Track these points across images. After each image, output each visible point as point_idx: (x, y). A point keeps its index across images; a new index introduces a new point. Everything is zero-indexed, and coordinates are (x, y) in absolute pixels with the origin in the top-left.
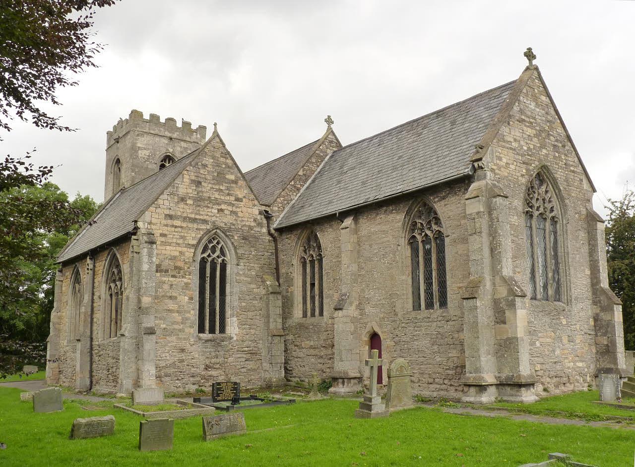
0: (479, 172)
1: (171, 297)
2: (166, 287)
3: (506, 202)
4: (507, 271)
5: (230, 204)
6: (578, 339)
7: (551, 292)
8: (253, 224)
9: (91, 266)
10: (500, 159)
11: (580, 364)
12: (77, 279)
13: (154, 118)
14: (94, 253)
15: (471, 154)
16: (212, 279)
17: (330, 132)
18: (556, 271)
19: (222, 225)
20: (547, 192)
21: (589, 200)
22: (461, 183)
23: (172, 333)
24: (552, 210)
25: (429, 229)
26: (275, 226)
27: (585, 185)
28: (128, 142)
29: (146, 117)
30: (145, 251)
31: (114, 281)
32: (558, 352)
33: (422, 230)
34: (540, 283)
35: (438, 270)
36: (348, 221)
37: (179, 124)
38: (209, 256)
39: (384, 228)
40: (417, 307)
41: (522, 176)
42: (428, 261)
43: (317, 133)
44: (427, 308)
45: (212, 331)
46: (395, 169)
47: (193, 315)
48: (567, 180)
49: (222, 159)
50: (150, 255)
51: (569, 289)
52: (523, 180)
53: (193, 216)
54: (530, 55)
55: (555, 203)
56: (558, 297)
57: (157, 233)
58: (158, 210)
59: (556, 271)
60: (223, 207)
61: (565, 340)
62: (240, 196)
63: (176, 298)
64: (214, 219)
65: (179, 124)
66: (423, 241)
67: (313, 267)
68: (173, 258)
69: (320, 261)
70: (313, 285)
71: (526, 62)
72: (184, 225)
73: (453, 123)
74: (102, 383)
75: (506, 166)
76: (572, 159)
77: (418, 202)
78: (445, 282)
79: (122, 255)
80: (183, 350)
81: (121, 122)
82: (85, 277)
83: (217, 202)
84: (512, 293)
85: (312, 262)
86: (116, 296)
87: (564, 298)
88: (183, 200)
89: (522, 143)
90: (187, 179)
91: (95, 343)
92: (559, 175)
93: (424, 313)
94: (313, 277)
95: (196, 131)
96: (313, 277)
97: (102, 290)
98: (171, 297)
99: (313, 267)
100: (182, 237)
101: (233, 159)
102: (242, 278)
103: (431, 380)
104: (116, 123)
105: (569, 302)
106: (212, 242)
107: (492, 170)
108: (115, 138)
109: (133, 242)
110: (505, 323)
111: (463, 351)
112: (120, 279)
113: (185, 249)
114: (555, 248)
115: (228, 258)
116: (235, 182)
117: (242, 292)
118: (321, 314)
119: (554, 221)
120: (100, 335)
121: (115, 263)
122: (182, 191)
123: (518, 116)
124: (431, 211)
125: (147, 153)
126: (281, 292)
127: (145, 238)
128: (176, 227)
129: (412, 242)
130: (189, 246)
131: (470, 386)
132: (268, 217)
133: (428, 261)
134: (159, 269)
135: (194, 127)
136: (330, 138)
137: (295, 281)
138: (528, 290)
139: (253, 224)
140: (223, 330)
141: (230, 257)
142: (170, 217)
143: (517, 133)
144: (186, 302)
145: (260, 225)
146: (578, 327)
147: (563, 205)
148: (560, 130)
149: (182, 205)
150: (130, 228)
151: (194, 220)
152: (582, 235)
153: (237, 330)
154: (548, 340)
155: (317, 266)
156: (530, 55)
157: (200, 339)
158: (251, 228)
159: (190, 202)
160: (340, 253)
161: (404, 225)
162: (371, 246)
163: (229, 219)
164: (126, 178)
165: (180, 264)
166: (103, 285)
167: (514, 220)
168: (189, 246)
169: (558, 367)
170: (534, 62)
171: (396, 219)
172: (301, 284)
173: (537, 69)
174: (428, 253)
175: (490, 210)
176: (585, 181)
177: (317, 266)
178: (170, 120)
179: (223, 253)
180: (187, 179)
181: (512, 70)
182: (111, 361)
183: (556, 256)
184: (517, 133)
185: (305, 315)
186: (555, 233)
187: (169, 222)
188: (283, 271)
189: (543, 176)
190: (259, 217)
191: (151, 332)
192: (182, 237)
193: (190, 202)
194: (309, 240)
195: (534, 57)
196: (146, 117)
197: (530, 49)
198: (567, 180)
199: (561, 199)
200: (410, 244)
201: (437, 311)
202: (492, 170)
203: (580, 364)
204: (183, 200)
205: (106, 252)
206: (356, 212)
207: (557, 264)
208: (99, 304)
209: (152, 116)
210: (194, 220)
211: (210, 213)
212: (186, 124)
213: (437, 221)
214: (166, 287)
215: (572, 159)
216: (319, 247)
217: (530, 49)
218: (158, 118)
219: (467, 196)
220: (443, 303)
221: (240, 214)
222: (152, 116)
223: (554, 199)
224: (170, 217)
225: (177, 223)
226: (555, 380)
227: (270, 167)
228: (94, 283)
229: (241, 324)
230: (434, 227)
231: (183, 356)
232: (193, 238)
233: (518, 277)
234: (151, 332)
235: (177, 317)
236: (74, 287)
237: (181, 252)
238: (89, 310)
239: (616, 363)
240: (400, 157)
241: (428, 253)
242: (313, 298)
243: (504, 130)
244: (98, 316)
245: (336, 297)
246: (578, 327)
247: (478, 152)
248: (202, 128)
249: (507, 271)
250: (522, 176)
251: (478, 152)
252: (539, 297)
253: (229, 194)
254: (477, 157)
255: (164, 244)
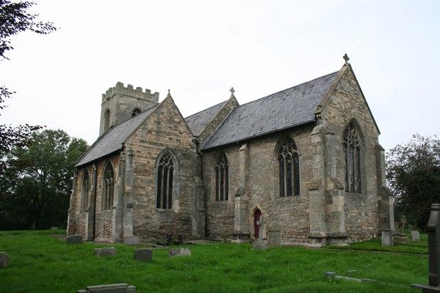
0: (320, 120)
1: (142, 187)
2: (139, 181)
3: (333, 137)
4: (334, 175)
5: (176, 135)
6: (370, 214)
7: (356, 188)
8: (189, 147)
9: (95, 169)
10: (330, 113)
11: (371, 228)
12: (86, 177)
13: (130, 87)
14: (97, 162)
15: (315, 110)
16: (164, 177)
17: (233, 97)
18: (359, 177)
19: (171, 147)
20: (354, 133)
21: (377, 138)
22: (307, 127)
23: (143, 207)
24: (357, 143)
25: (290, 151)
26: (201, 148)
27: (375, 130)
28: (115, 100)
29: (126, 86)
30: (128, 161)
31: (109, 178)
32: (359, 221)
33: (286, 152)
34: (350, 183)
35: (284, 190)
36: (244, 147)
37: (144, 91)
38: (164, 164)
39: (264, 150)
40: (282, 195)
41: (342, 123)
42: (289, 169)
43: (226, 97)
44: (288, 196)
45: (164, 207)
46: (271, 118)
47: (154, 197)
48: (365, 127)
49: (172, 110)
50: (131, 163)
51: (366, 186)
52: (342, 126)
53: (155, 141)
54: (346, 58)
55: (359, 139)
56: (359, 191)
57: (135, 150)
58: (136, 138)
59: (359, 177)
60: (172, 137)
61: (363, 214)
62: (182, 131)
63: (144, 188)
64: (167, 143)
65: (144, 91)
66: (286, 158)
67: (222, 173)
68: (144, 165)
69: (227, 169)
70: (222, 183)
71: (344, 62)
72: (150, 146)
73: (304, 93)
74: (101, 235)
75: (334, 118)
76: (368, 115)
77: (284, 138)
78: (299, 181)
79: (114, 163)
80: (148, 218)
81: (111, 89)
82: (91, 176)
83: (169, 134)
84: (336, 186)
85: (222, 170)
86: (110, 187)
87: (363, 191)
88: (150, 132)
89: (343, 105)
90: (152, 121)
91: (97, 213)
92: (361, 123)
93: (287, 199)
94: (222, 178)
95: (153, 95)
96: (222, 178)
97: (101, 183)
98: (142, 187)
99: (222, 173)
100: (149, 153)
101: (178, 110)
102: (182, 177)
103: (290, 236)
104: (108, 90)
105: (366, 194)
106: (166, 157)
107: (326, 119)
108: (107, 98)
109: (122, 155)
110: (332, 203)
111: (308, 219)
112: (113, 177)
113: (150, 160)
114: (359, 164)
115: (174, 166)
116: (179, 123)
117: (181, 186)
118: (227, 199)
119: (358, 149)
120: (100, 208)
121: (110, 168)
122: (150, 127)
123: (340, 90)
124: (291, 141)
125: (126, 106)
126: (203, 189)
127: (129, 153)
128: (145, 147)
129: (280, 158)
130: (152, 158)
131: (312, 238)
132: (197, 143)
133: (289, 169)
134: (136, 171)
135: (152, 93)
136: (233, 101)
137: (212, 180)
138: (344, 186)
139: (189, 147)
140: (170, 207)
141: (175, 165)
142: (143, 141)
143: (339, 100)
144: (150, 190)
145: (193, 148)
146: (370, 207)
147: (363, 141)
148: (362, 100)
149: (149, 135)
150: (120, 147)
151: (155, 144)
152: (373, 157)
153: (178, 208)
154: (355, 214)
155: (225, 172)
156: (346, 58)
157: (158, 211)
158: (188, 149)
159: (154, 133)
160: (239, 164)
161: (275, 149)
162: (256, 161)
163: (176, 144)
164: (112, 119)
165: (147, 168)
166: (102, 180)
167: (338, 147)
168: (152, 158)
169: (360, 229)
170: (348, 62)
171: (272, 146)
172: (215, 182)
173: (350, 65)
174: (289, 165)
175: (324, 141)
176: (375, 127)
177: (225, 172)
178: (139, 89)
179: (171, 163)
180: (152, 121)
181: (337, 66)
182: (106, 223)
183: (359, 169)
184: (339, 100)
185: (217, 199)
186: (359, 155)
187: (142, 144)
188: (205, 175)
189: (353, 124)
190: (192, 143)
191: (130, 206)
192: (149, 153)
193: (154, 133)
194: (220, 157)
195: (348, 59)
196: (126, 86)
197: (346, 55)
198: (365, 127)
199: (362, 137)
200: (279, 159)
201: (293, 198)
202: (326, 119)
203: (371, 228)
204: (150, 132)
205: (105, 161)
206: (250, 141)
207: (359, 172)
208: (99, 190)
209: (129, 86)
210: (155, 144)
211: (165, 140)
212: (148, 91)
213: (295, 147)
214: (139, 181)
215: (368, 115)
216: (226, 161)
217: (346, 55)
218: (132, 87)
219: (312, 133)
220: (297, 193)
221: (182, 141)
222: (129, 86)
223: (359, 137)
224: (143, 141)
225: (147, 145)
226: (357, 236)
227: (197, 116)
228: (97, 178)
229: (181, 205)
230: (293, 151)
231: (148, 220)
232: (155, 154)
233: (339, 179)
234: (130, 206)
235: (146, 199)
236: (84, 182)
237: (148, 162)
238: (94, 193)
239: (389, 227)
240: (273, 111)
241: (289, 165)
242: (222, 190)
243: (333, 98)
244: (99, 197)
245: (236, 189)
246: (370, 207)
247: (318, 109)
248: (157, 94)
249: (334, 175)
250: (342, 123)
251: (318, 109)
252: (350, 190)
253: (176, 130)
254: (318, 111)
255: (139, 156)
